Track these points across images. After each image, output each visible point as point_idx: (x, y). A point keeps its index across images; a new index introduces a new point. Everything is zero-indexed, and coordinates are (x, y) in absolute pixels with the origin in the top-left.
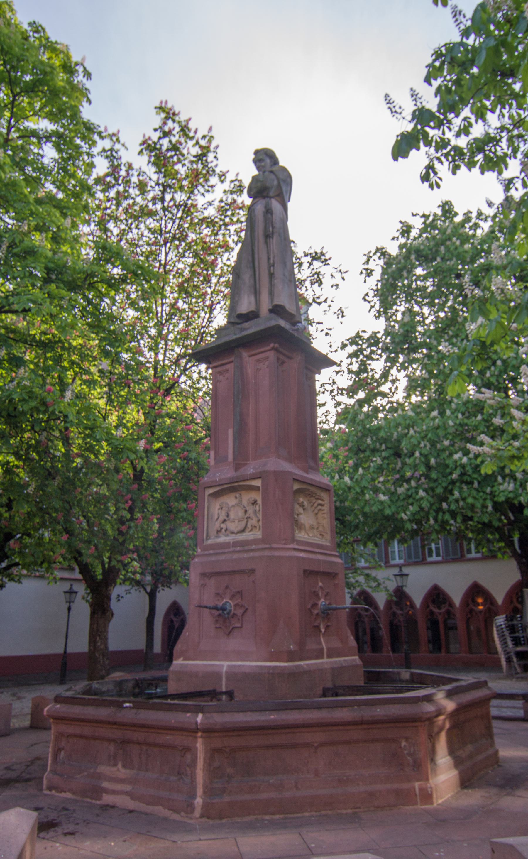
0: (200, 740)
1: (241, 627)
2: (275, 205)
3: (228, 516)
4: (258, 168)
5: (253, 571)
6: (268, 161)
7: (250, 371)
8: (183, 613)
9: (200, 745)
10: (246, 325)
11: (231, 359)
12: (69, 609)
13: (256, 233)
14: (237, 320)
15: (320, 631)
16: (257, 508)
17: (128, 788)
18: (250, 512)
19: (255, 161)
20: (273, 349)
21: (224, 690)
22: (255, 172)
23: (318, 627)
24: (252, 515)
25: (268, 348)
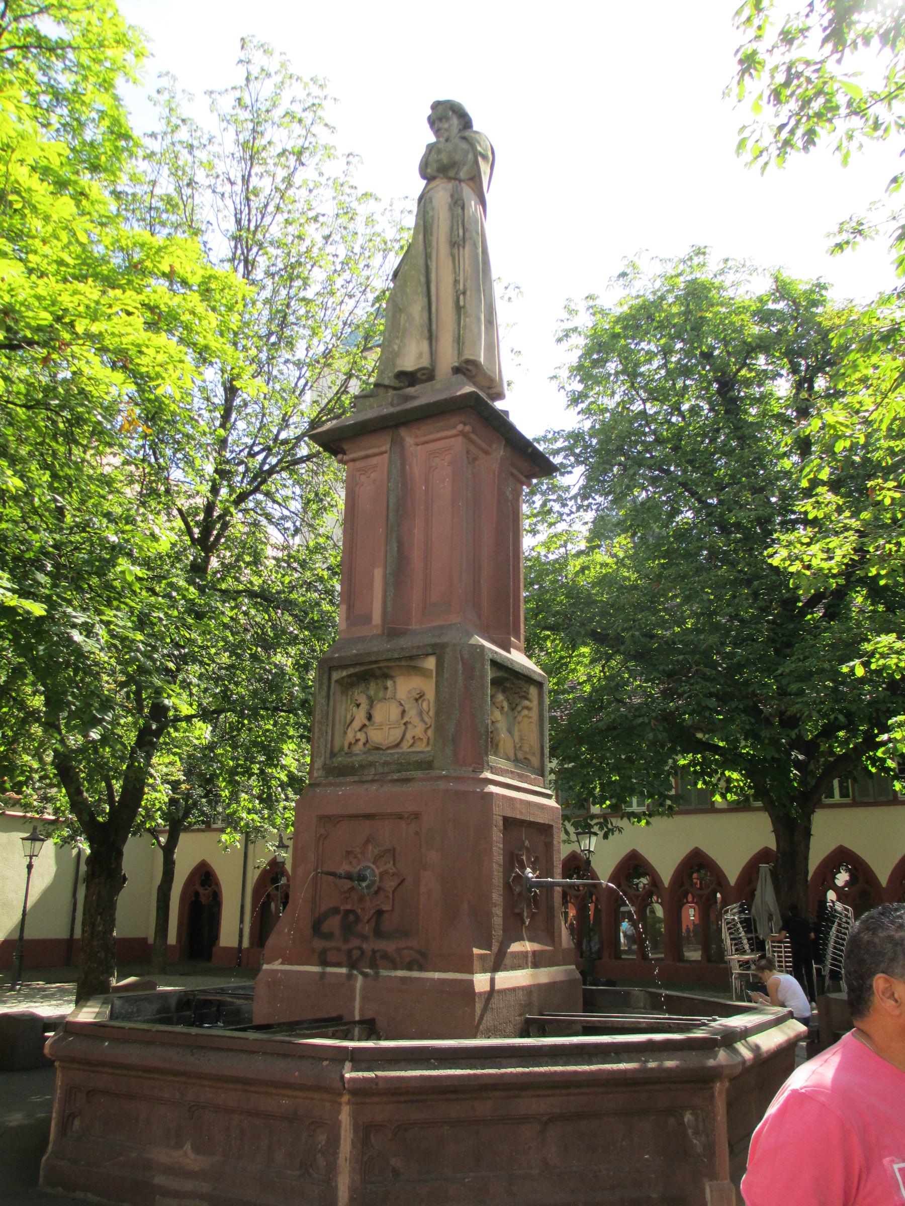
1: (392, 911)
2: (467, 191)
3: (370, 717)
4: (437, 132)
5: (416, 816)
6: (455, 121)
7: (417, 470)
8: (217, 884)
9: (345, 1117)
10: (410, 391)
11: (383, 449)
12: (30, 867)
13: (434, 239)
14: (397, 384)
15: (524, 923)
16: (425, 705)
17: (205, 1187)
18: (412, 714)
19: (432, 122)
21: (357, 1018)
22: (432, 139)
23: (520, 916)
25: (454, 432)
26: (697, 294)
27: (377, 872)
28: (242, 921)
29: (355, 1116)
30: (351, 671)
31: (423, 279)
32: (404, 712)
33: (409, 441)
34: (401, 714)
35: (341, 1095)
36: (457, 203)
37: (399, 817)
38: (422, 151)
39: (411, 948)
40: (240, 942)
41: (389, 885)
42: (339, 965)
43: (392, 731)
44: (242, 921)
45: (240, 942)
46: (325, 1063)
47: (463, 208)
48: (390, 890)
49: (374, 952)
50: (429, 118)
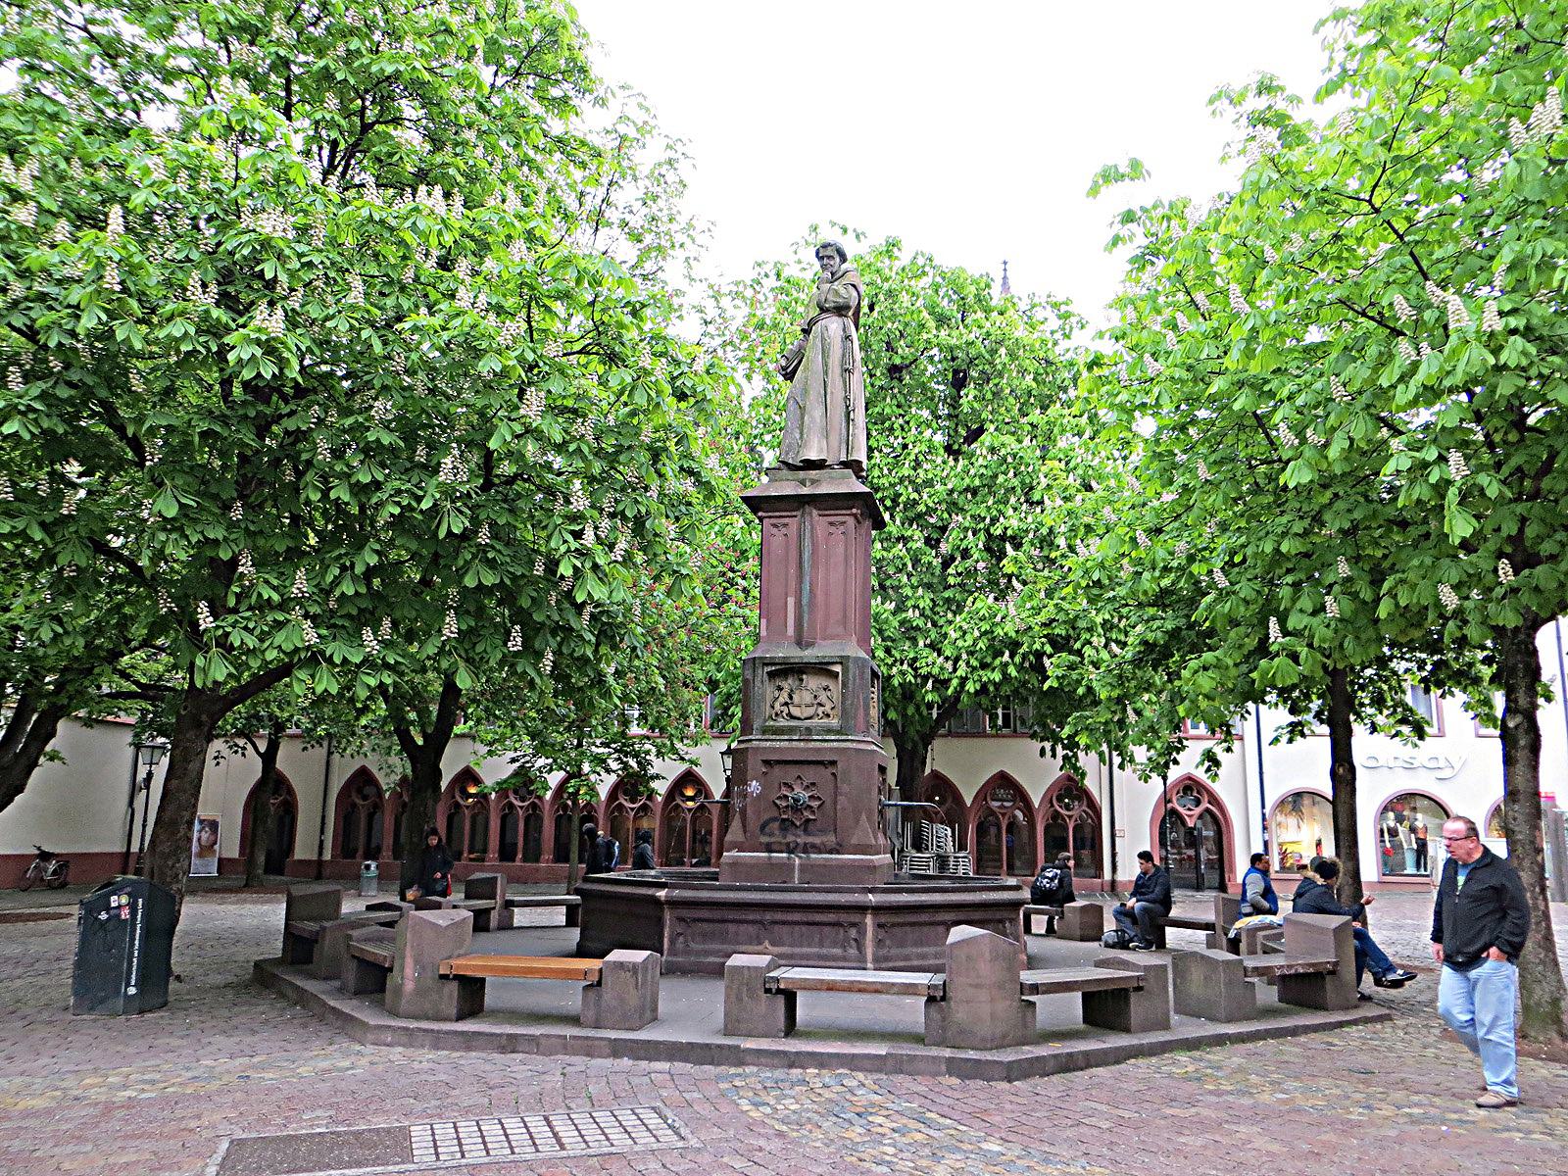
5: (833, 763)
8: (290, 791)
40: (320, 853)
45: (320, 853)
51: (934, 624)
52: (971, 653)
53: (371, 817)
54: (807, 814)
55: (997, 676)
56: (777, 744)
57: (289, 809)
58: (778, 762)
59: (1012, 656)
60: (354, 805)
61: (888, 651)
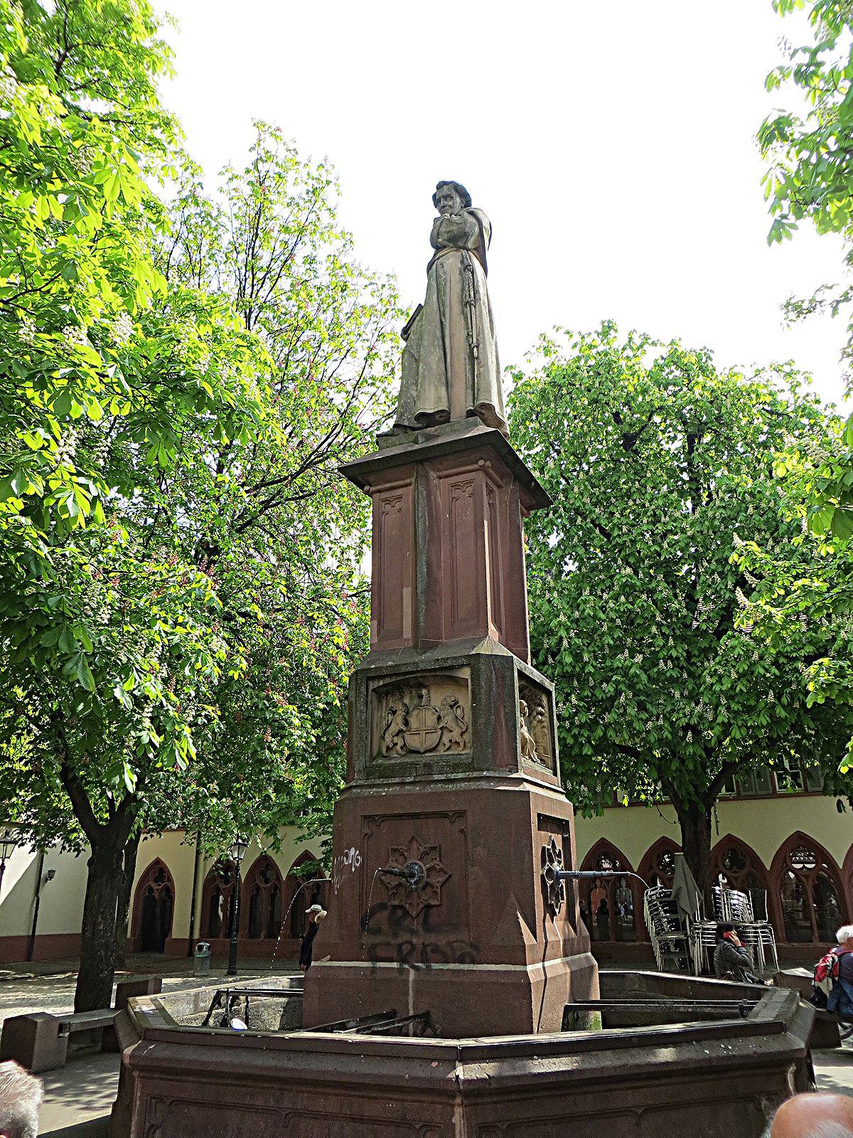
0: (458, 1111)
3: (406, 723)
5: (461, 814)
7: (441, 499)
8: (170, 879)
9: (458, 1119)
11: (408, 481)
13: (447, 298)
18: (448, 720)
20: (482, 468)
21: (411, 1013)
24: (451, 725)
25: (476, 466)
26: (606, 368)
27: (424, 868)
28: (193, 914)
29: (466, 1116)
30: (388, 680)
31: (439, 334)
32: (439, 718)
33: (433, 475)
34: (437, 721)
35: (454, 1097)
36: (467, 268)
37: (444, 815)
38: (430, 226)
39: (463, 942)
40: (192, 933)
41: (437, 880)
42: (391, 960)
43: (429, 735)
44: (193, 914)
45: (192, 933)
46: (434, 1064)
47: (473, 273)
48: (439, 885)
49: (425, 946)
50: (434, 196)
51: (691, 674)
52: (731, 698)
53: (273, 897)
54: (426, 897)
55: (764, 720)
56: (384, 792)
57: (169, 892)
58: (385, 817)
59: (778, 696)
60: (258, 888)
61: (641, 707)
